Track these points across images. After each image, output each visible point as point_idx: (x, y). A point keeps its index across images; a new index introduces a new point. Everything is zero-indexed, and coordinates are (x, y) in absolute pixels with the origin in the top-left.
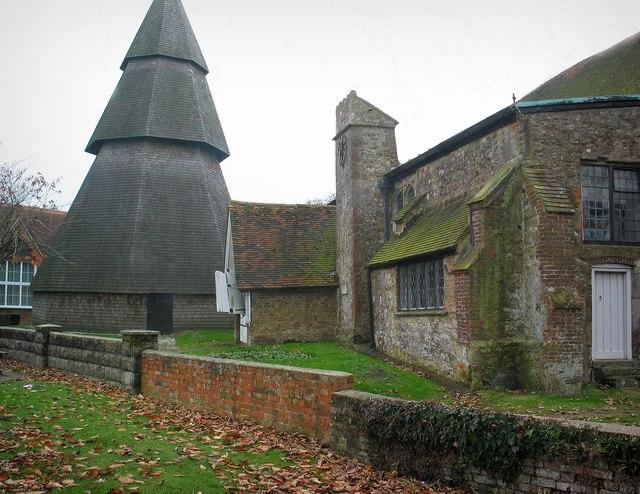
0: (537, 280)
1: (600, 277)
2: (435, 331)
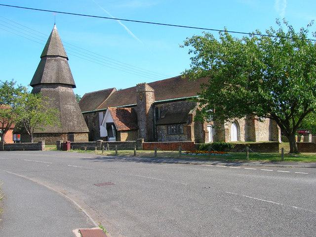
2: (181, 137)
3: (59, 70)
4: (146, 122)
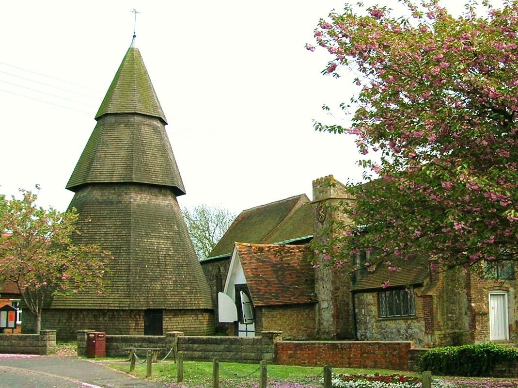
0: (465, 300)
1: (492, 297)
2: (409, 327)
3: (136, 148)
4: (333, 282)
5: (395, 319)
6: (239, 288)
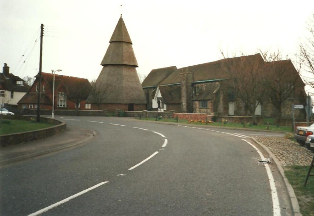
5: (203, 109)
6: (159, 99)
